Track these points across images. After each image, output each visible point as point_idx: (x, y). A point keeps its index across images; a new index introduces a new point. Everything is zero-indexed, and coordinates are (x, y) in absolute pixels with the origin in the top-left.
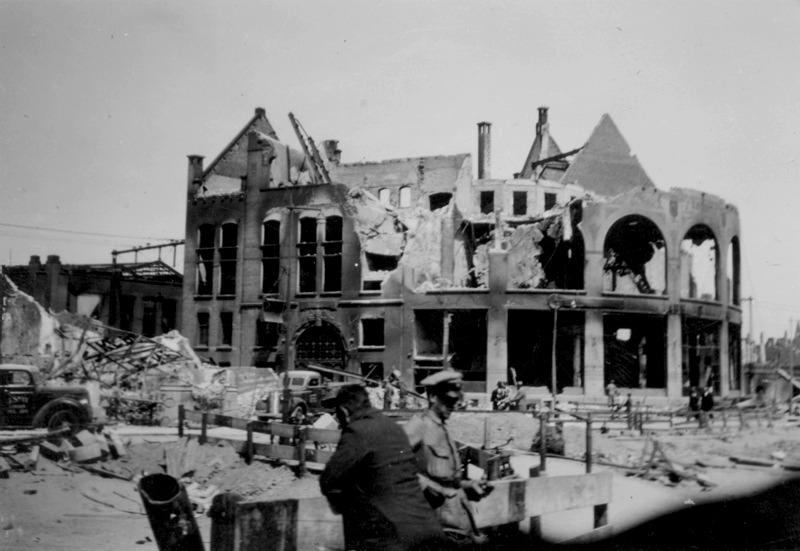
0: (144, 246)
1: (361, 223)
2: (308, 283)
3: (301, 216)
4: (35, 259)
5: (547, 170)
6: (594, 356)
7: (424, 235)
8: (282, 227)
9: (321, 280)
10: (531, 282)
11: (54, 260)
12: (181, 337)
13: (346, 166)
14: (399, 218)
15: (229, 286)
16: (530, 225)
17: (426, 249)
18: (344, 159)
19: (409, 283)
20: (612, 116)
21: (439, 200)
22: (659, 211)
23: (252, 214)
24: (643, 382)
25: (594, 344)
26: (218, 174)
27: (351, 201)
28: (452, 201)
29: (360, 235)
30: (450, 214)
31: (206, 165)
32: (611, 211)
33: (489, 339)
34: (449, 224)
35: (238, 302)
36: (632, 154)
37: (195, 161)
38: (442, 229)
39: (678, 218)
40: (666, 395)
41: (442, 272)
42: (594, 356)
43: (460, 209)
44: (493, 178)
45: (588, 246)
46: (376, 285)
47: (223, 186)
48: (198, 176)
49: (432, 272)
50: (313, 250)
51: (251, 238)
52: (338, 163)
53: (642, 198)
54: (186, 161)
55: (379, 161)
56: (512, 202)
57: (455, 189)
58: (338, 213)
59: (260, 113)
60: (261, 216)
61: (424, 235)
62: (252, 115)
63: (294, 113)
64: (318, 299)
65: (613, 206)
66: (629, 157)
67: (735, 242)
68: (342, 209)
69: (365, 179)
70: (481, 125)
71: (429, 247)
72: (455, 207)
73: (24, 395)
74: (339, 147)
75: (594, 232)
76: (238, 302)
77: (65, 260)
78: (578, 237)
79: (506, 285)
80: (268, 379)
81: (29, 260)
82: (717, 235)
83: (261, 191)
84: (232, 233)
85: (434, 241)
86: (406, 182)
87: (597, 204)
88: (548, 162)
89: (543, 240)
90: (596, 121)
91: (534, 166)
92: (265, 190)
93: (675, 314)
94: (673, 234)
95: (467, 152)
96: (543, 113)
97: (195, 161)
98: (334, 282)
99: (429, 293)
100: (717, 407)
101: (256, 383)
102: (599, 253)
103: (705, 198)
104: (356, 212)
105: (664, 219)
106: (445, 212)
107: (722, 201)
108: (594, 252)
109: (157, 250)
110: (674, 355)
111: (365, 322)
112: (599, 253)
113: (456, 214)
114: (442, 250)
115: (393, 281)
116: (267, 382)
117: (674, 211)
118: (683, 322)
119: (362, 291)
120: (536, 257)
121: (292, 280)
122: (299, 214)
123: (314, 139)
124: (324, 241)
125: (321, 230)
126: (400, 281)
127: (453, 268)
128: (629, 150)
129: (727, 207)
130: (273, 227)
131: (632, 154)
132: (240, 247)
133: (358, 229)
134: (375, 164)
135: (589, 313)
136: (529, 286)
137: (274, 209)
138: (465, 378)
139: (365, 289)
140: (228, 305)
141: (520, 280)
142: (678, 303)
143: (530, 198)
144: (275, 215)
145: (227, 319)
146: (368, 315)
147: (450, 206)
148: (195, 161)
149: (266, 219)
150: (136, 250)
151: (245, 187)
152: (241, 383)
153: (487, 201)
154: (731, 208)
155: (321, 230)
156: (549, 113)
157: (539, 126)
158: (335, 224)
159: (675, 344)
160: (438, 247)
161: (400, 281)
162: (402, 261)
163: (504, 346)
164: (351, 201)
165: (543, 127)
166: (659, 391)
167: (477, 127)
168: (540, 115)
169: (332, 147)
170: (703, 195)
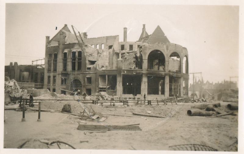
0: (38, 59)
1: (87, 53)
2: (74, 68)
3: (72, 51)
4: (11, 63)
5: (145, 40)
6: (144, 87)
7: (103, 56)
8: (67, 54)
9: (76, 68)
10: (132, 68)
11: (16, 63)
12: (15, 81)
13: (88, 39)
14: (99, 52)
15: (55, 70)
16: (132, 53)
17: (104, 59)
18: (88, 37)
19: (98, 68)
20: (160, 26)
21: (110, 47)
22: (163, 49)
23: (61, 51)
24: (160, 93)
25: (145, 83)
26: (54, 41)
27: (84, 47)
28: (112, 47)
29: (86, 56)
30: (112, 50)
31: (50, 39)
32: (150, 49)
33: (117, 82)
34: (112, 53)
35: (57, 73)
36: (165, 35)
37: (48, 38)
38: (109, 54)
39: (169, 51)
40: (165, 96)
41: (109, 65)
42: (144, 87)
43: (115, 49)
44: (127, 41)
45: (144, 58)
46: (89, 69)
47: (55, 44)
48: (48, 41)
49: (106, 65)
50: (75, 60)
51: (60, 57)
52: (87, 38)
53: (158, 46)
54: (45, 38)
55: (96, 37)
56: (129, 47)
57: (114, 44)
58: (81, 50)
59: (66, 25)
60: (63, 50)
61: (103, 56)
62: (63, 26)
63: (73, 25)
64: (76, 72)
65: (150, 48)
66: (164, 36)
67: (187, 56)
68: (82, 49)
69: (93, 42)
70: (124, 28)
71: (105, 59)
72: (113, 49)
73: (170, 86)
74: (87, 34)
75: (145, 54)
76: (57, 73)
77: (19, 64)
78: (141, 56)
79: (122, 68)
80: (47, 92)
81: (10, 63)
82: (180, 56)
83: (63, 45)
84: (56, 56)
85: (107, 57)
86: (103, 43)
87: (146, 47)
88: (144, 37)
89: (135, 57)
90: (156, 27)
91: (142, 39)
92: (64, 44)
93: (167, 75)
94: (167, 55)
95: (118, 35)
96: (144, 25)
97: (48, 38)
98: (79, 68)
99: (102, 70)
100: (94, 112)
101: (44, 93)
102: (146, 60)
103: (176, 45)
104: (85, 50)
105: (164, 51)
106: (111, 50)
107: (181, 46)
108: (145, 60)
109: (36, 62)
110: (167, 86)
111: (87, 78)
112: (146, 60)
113: (114, 50)
114: (109, 60)
115: (93, 67)
116: (47, 93)
117: (167, 49)
118: (169, 77)
119: (87, 70)
120: (134, 61)
121: (69, 67)
122: (71, 51)
123: (80, 32)
124: (77, 57)
125: (77, 54)
126: (95, 67)
127: (113, 64)
128: (164, 35)
129: (183, 48)
130: (65, 54)
131: (165, 35)
132: (58, 59)
133: (85, 54)
134: (95, 38)
135: (143, 75)
136: (132, 69)
137: (66, 49)
138: (183, 87)
139: (87, 69)
140: (55, 74)
141: (130, 67)
142: (168, 73)
143: (134, 46)
144: (66, 51)
145: (54, 77)
146: (88, 76)
147: (112, 49)
148: (48, 38)
149: (64, 52)
150: (37, 61)
151: (59, 44)
152: (41, 93)
153: (123, 47)
154: (185, 49)
155: (77, 54)
156: (146, 26)
157: (143, 29)
158: (80, 53)
159: (167, 83)
160: (108, 59)
161: (95, 67)
162: (96, 63)
163: (121, 84)
164: (84, 47)
165: (144, 29)
166: (140, 95)
167: (123, 29)
168: (143, 26)
169: (85, 34)
170: (176, 44)
